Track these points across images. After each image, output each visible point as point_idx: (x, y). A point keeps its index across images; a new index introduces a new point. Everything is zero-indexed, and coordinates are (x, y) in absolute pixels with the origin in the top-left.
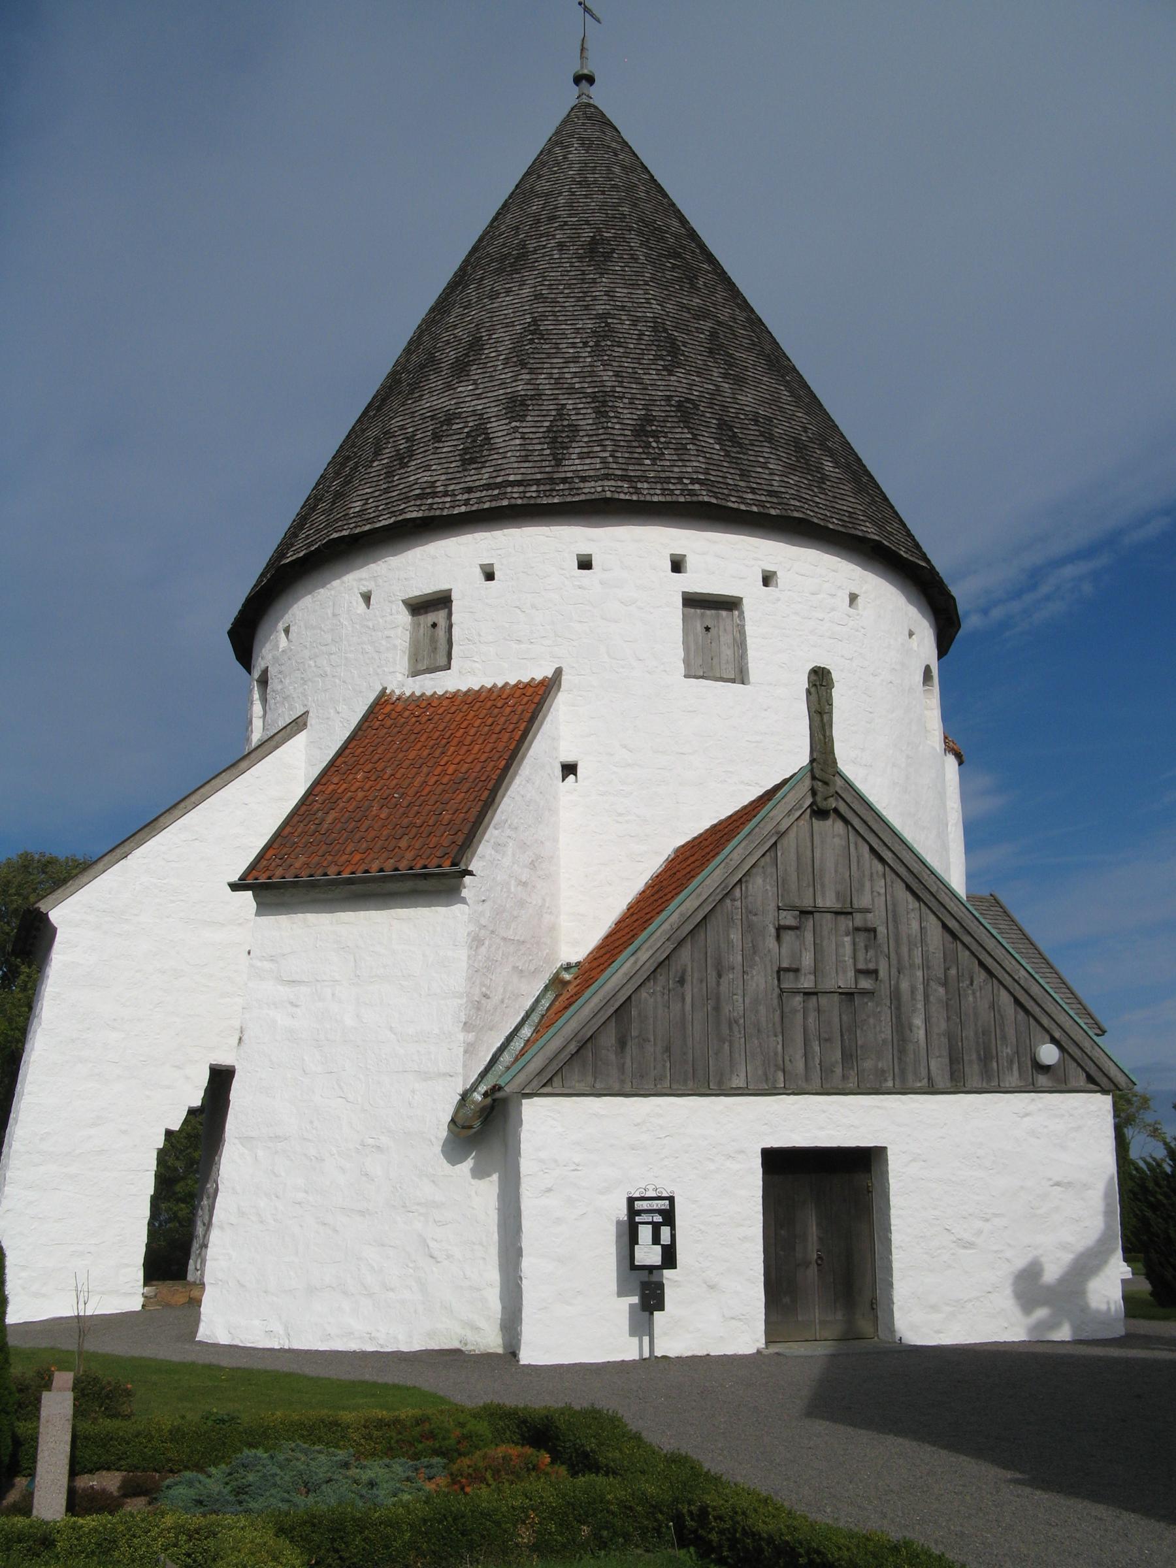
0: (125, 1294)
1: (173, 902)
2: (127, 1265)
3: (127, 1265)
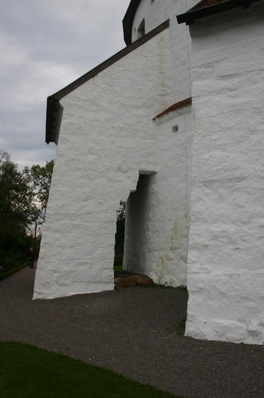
0: (106, 282)
1: (116, 97)
2: (106, 268)
3: (106, 268)
